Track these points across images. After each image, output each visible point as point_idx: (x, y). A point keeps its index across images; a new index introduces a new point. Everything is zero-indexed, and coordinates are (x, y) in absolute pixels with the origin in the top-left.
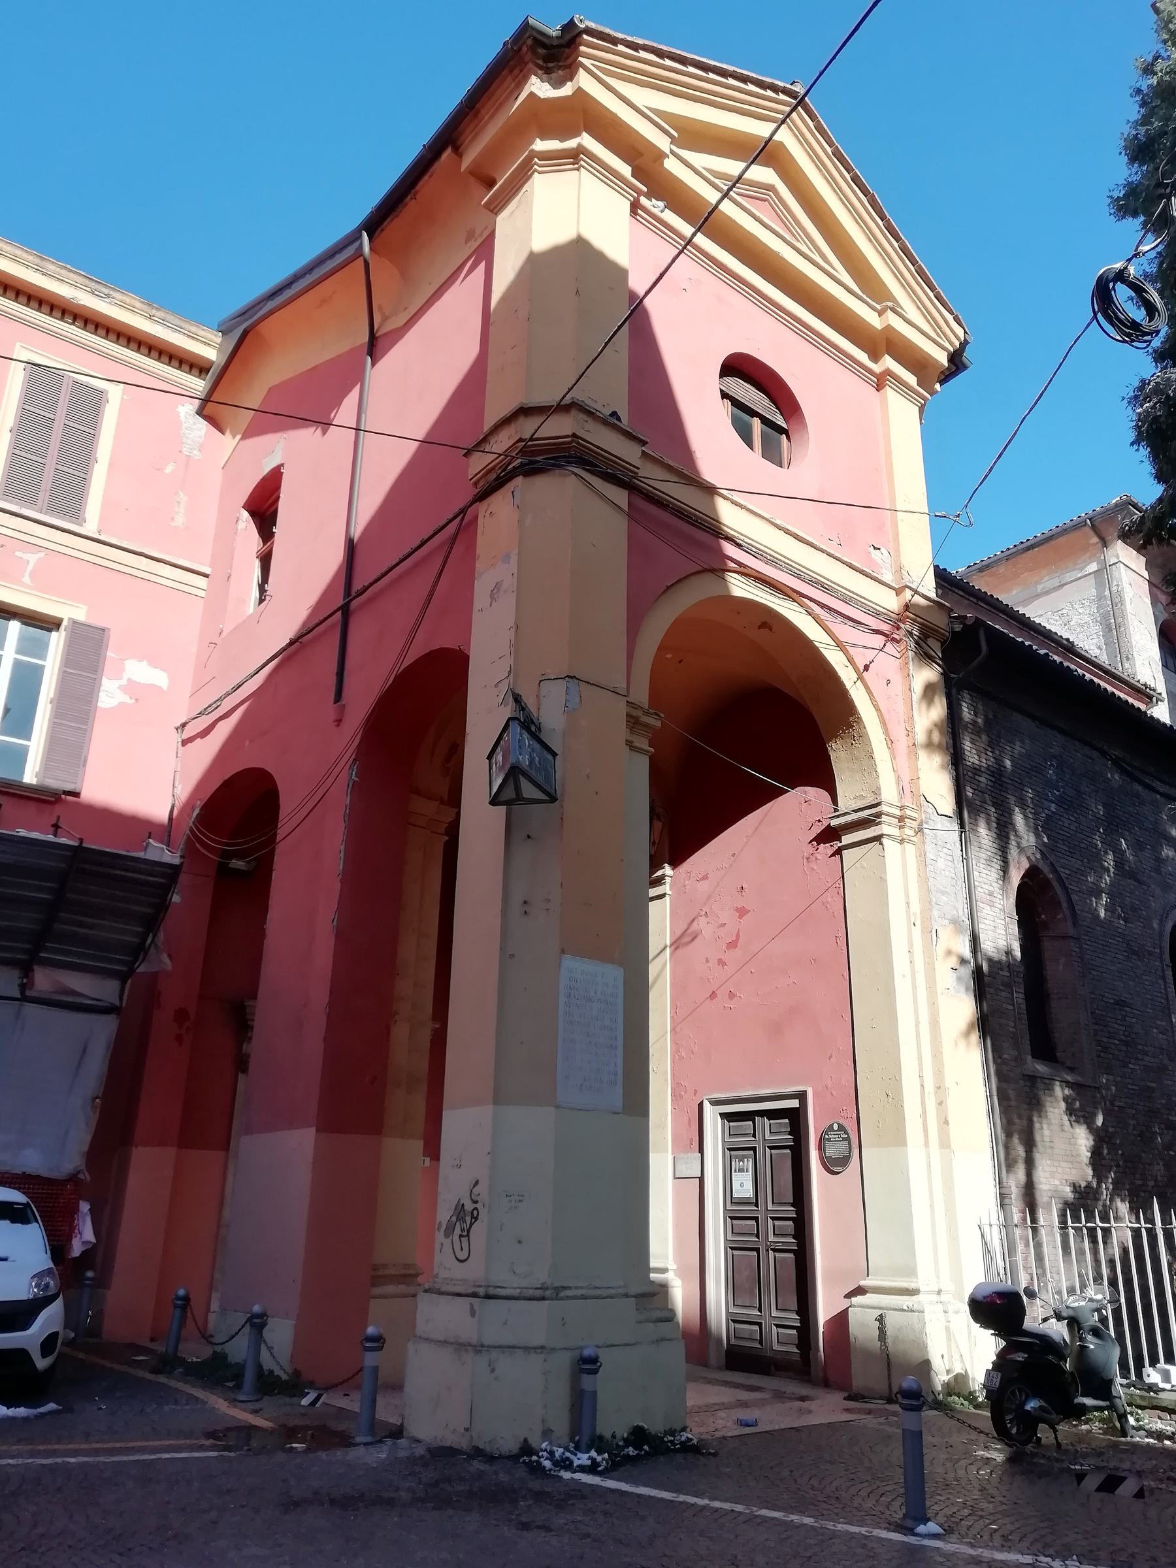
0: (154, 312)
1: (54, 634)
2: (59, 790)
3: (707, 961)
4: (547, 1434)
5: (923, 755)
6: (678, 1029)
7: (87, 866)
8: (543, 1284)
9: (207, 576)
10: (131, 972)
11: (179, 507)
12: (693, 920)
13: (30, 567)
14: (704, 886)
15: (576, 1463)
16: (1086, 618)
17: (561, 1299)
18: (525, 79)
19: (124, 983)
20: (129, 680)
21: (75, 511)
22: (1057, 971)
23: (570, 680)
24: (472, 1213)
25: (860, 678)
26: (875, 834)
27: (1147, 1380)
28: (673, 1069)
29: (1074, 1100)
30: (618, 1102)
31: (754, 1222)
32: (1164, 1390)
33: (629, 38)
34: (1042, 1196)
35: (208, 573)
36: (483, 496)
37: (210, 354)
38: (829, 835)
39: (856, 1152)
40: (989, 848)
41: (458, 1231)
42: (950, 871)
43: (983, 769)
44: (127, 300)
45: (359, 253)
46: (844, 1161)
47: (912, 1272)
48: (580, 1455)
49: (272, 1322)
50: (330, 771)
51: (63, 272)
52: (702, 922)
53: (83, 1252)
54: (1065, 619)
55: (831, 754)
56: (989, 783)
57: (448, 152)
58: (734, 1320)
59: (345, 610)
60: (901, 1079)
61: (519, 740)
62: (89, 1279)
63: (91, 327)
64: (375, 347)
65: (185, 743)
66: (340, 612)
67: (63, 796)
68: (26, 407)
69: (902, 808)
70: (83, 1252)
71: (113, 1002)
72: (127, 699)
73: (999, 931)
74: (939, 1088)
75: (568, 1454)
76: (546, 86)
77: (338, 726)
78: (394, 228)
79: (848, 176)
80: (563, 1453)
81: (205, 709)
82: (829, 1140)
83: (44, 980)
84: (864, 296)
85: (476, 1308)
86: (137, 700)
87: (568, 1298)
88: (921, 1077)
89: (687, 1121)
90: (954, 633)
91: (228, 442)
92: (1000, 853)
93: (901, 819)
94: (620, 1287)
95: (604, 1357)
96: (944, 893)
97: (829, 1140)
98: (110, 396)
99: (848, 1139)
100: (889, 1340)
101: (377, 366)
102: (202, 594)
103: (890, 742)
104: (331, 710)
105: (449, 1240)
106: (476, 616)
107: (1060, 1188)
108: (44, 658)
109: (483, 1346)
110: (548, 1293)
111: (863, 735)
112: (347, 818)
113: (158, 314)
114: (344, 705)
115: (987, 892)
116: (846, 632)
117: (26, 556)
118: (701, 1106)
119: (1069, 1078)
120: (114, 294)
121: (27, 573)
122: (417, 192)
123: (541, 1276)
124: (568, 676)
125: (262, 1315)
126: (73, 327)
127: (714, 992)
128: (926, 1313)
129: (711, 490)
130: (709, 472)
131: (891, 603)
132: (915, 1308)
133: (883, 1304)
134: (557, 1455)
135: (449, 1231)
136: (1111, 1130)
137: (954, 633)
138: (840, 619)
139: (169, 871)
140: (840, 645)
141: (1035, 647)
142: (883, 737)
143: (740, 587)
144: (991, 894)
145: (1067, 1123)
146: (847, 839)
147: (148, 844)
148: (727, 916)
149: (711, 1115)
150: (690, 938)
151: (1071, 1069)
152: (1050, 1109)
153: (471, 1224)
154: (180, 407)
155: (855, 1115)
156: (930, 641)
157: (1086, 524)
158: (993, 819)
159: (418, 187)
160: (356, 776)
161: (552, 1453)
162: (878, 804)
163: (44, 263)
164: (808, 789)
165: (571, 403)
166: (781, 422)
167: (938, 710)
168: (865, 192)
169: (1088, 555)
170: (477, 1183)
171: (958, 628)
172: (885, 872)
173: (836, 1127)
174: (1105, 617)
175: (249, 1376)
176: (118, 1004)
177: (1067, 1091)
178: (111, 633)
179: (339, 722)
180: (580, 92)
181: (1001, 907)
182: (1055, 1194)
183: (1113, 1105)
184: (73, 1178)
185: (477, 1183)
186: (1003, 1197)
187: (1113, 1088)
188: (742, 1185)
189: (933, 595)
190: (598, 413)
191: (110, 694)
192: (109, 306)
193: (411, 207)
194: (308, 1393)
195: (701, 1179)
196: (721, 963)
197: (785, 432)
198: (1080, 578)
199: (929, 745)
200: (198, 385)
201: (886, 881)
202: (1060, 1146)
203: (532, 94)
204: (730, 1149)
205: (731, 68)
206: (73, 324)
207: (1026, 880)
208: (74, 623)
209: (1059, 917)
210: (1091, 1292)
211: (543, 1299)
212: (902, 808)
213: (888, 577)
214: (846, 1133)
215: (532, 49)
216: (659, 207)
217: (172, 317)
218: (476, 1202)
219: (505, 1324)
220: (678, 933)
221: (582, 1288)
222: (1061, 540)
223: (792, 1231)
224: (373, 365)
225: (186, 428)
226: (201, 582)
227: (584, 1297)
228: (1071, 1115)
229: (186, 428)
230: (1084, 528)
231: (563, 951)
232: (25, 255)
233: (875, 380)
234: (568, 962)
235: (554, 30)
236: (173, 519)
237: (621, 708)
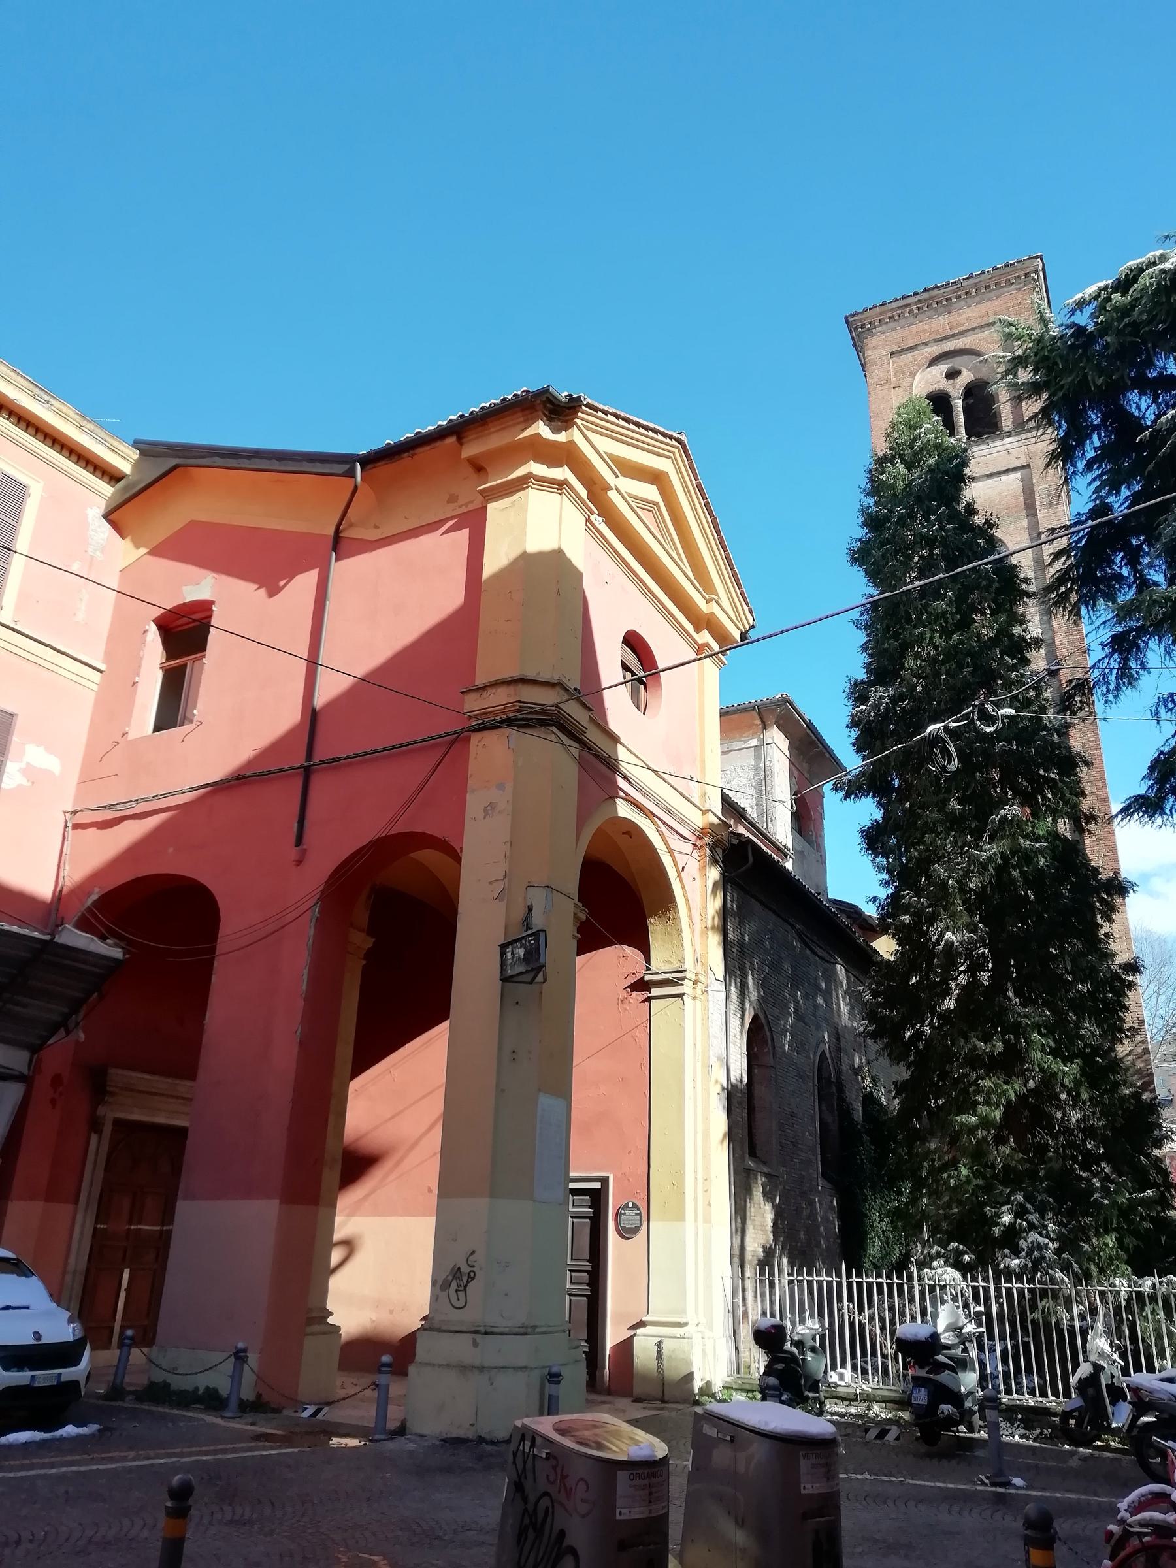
0: (84, 423)
5: (710, 933)
7: (67, 962)
8: (523, 1324)
9: (101, 671)
16: (745, 782)
18: (534, 421)
24: (469, 1273)
25: (679, 876)
27: (831, 1380)
29: (767, 1185)
32: (840, 1386)
34: (748, 1256)
37: (126, 468)
38: (641, 985)
39: (645, 1224)
41: (454, 1286)
43: (735, 943)
44: (64, 409)
46: (635, 1230)
47: (683, 1312)
50: (297, 905)
51: (13, 374)
54: (728, 778)
55: (650, 928)
60: (684, 1173)
63: (23, 425)
69: (697, 974)
71: (22, 1071)
72: (25, 782)
74: (706, 1180)
77: (298, 865)
78: (384, 470)
79: (702, 502)
82: (624, 1214)
84: (701, 589)
85: (478, 1341)
86: (33, 783)
88: (696, 1172)
92: (740, 1005)
93: (695, 982)
97: (624, 1214)
99: (640, 1214)
103: (692, 924)
104: (293, 853)
105: (446, 1293)
109: (484, 1367)
110: (529, 1330)
111: (676, 918)
114: (306, 850)
120: (53, 401)
122: (416, 454)
124: (548, 887)
125: (245, 1351)
128: (693, 1340)
129: (614, 739)
130: (614, 725)
131: (699, 821)
132: (686, 1336)
133: (662, 1334)
136: (783, 1207)
138: (676, 836)
140: (671, 852)
142: (688, 919)
143: (623, 810)
145: (762, 1202)
146: (655, 992)
152: (755, 1193)
153: (468, 1282)
154: (89, 509)
155: (646, 1197)
156: (718, 849)
157: (754, 709)
159: (417, 451)
164: (625, 947)
168: (711, 515)
169: (751, 732)
170: (473, 1253)
171: (735, 842)
172: (683, 1021)
173: (630, 1205)
174: (759, 783)
175: (233, 1403)
178: (19, 718)
182: (754, 1251)
183: (784, 1188)
185: (473, 1253)
193: (406, 461)
194: (307, 1408)
198: (743, 749)
199: (713, 928)
200: (107, 490)
201: (683, 1027)
206: (8, 419)
209: (765, 1051)
210: (809, 1323)
211: (525, 1334)
212: (697, 974)
213: (696, 800)
214: (639, 1209)
215: (544, 403)
217: (99, 431)
218: (473, 1266)
219: (499, 1351)
222: (735, 716)
224: (337, 560)
225: (92, 530)
226: (97, 677)
227: (545, 1333)
229: (92, 530)
230: (752, 712)
231: (540, 1090)
235: (563, 396)
236: (75, 614)
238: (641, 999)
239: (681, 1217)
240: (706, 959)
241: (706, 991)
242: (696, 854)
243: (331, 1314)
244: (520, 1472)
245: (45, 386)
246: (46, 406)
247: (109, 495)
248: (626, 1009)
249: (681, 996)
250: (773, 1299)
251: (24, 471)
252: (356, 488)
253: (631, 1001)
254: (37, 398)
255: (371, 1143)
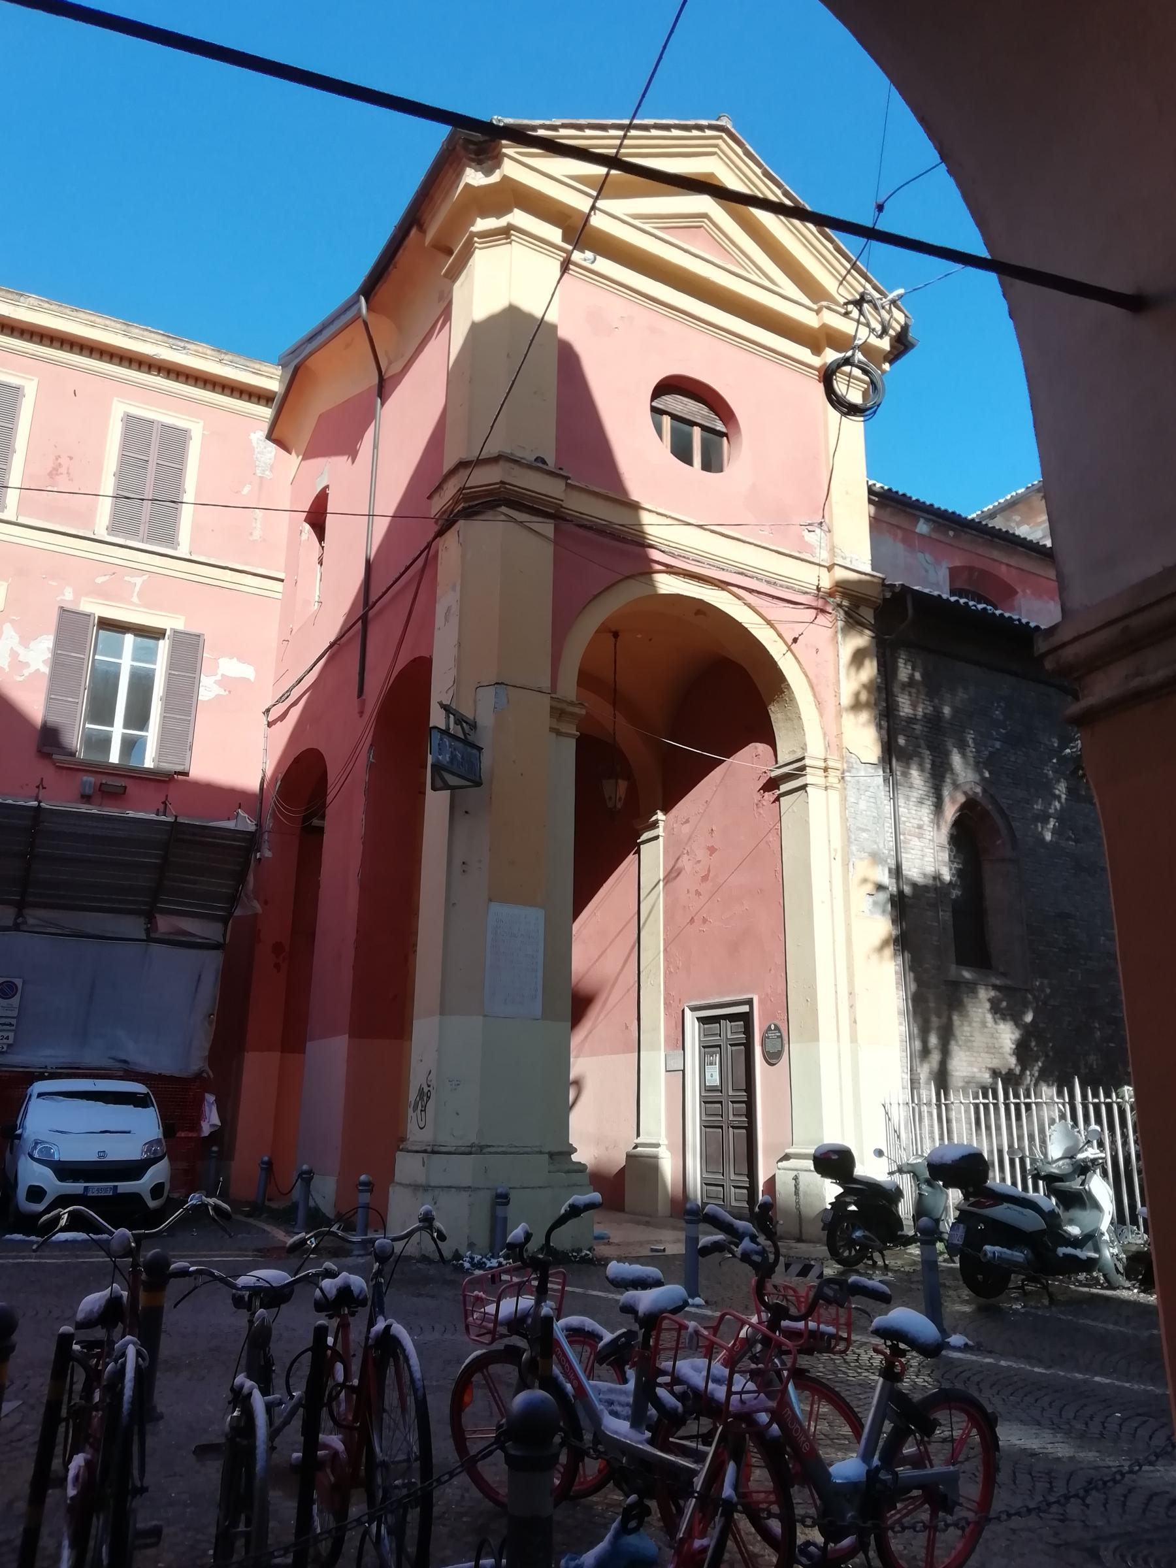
1: (161, 642)
2: (170, 772)
3: (688, 891)
4: (471, 1246)
6: (668, 949)
9: (282, 581)
10: (231, 914)
11: (256, 523)
12: (678, 859)
13: (137, 589)
14: (686, 829)
15: (489, 1265)
17: (484, 1154)
19: (226, 924)
20: (223, 675)
21: (170, 538)
22: (996, 891)
23: (498, 686)
26: (802, 784)
28: (665, 983)
29: (1001, 1001)
30: (538, 1011)
31: (719, 1105)
33: (548, 122)
35: (283, 577)
36: (440, 533)
38: (771, 785)
40: (921, 787)
42: (872, 811)
44: (200, 349)
45: (359, 315)
48: (492, 1260)
49: (317, 1180)
51: (146, 333)
52: (685, 858)
53: (211, 1133)
55: (771, 715)
56: (925, 729)
57: (414, 231)
58: (706, 1183)
59: (364, 619)
61: (439, 744)
62: (215, 1152)
64: (383, 388)
65: (270, 725)
66: (360, 621)
67: (175, 776)
68: (125, 453)
69: (825, 760)
70: (212, 1133)
72: (222, 692)
73: (927, 859)
75: (484, 1260)
76: (480, 174)
78: (384, 291)
80: (481, 1259)
81: (281, 698)
82: (768, 1038)
83: (164, 924)
86: (230, 692)
87: (490, 1153)
89: (674, 1025)
90: (885, 599)
91: (293, 461)
93: (826, 770)
94: (536, 1147)
95: (513, 1196)
96: (864, 830)
97: (768, 1038)
98: (193, 434)
99: (781, 1037)
100: (801, 1195)
101: (385, 406)
102: (279, 596)
103: (819, 703)
106: (437, 633)
107: (978, 1075)
108: (154, 662)
111: (792, 699)
112: (366, 793)
113: (226, 357)
115: (916, 826)
116: (778, 612)
117: (133, 580)
118: (683, 1011)
119: (998, 982)
120: (188, 346)
121: (135, 594)
123: (472, 1138)
125: (310, 1172)
126: (159, 378)
127: (692, 918)
129: (635, 507)
134: (476, 1260)
135: (415, 1110)
136: (1041, 1025)
137: (885, 599)
139: (248, 837)
141: (971, 603)
143: (667, 584)
144: (920, 827)
146: (784, 788)
147: (238, 813)
148: (701, 854)
149: (690, 1018)
150: (676, 874)
151: (1004, 975)
155: (786, 1017)
158: (928, 761)
160: (373, 758)
161: (472, 1258)
162: (803, 758)
163: (130, 328)
165: (499, 455)
166: (720, 427)
167: (869, 670)
176: (222, 941)
177: (992, 993)
179: (361, 713)
180: (505, 178)
181: (930, 838)
184: (198, 1076)
186: (914, 1083)
187: (1048, 991)
188: (712, 1076)
189: (868, 569)
190: (523, 461)
191: (208, 689)
192: (185, 356)
193: (394, 274)
195: (684, 1071)
196: (698, 893)
197: (725, 435)
199: (856, 706)
200: (266, 412)
202: (979, 1040)
203: (467, 185)
204: (704, 1047)
205: (651, 122)
207: (965, 811)
208: (175, 632)
211: (470, 1153)
214: (780, 1032)
216: (589, 260)
217: (238, 359)
220: (669, 869)
221: (502, 1146)
223: (744, 1111)
225: (258, 453)
226: (278, 586)
228: (996, 1013)
229: (258, 453)
231: (490, 900)
232: (113, 324)
233: (817, 373)
234: (495, 907)
236: (251, 534)
237: (546, 701)
238: (772, 800)
239: (815, 1038)
240: (841, 740)
241: (843, 778)
242: (822, 619)
243: (575, 1150)
244: (211, 1279)
245: (177, 331)
246: (184, 351)
247: (269, 416)
248: (760, 814)
249: (804, 787)
250: (968, 1125)
251: (184, 417)
252: (366, 324)
253: (765, 803)
254: (174, 347)
255: (587, 986)
